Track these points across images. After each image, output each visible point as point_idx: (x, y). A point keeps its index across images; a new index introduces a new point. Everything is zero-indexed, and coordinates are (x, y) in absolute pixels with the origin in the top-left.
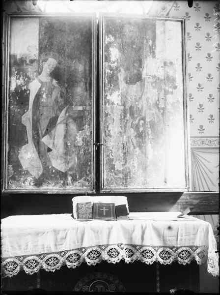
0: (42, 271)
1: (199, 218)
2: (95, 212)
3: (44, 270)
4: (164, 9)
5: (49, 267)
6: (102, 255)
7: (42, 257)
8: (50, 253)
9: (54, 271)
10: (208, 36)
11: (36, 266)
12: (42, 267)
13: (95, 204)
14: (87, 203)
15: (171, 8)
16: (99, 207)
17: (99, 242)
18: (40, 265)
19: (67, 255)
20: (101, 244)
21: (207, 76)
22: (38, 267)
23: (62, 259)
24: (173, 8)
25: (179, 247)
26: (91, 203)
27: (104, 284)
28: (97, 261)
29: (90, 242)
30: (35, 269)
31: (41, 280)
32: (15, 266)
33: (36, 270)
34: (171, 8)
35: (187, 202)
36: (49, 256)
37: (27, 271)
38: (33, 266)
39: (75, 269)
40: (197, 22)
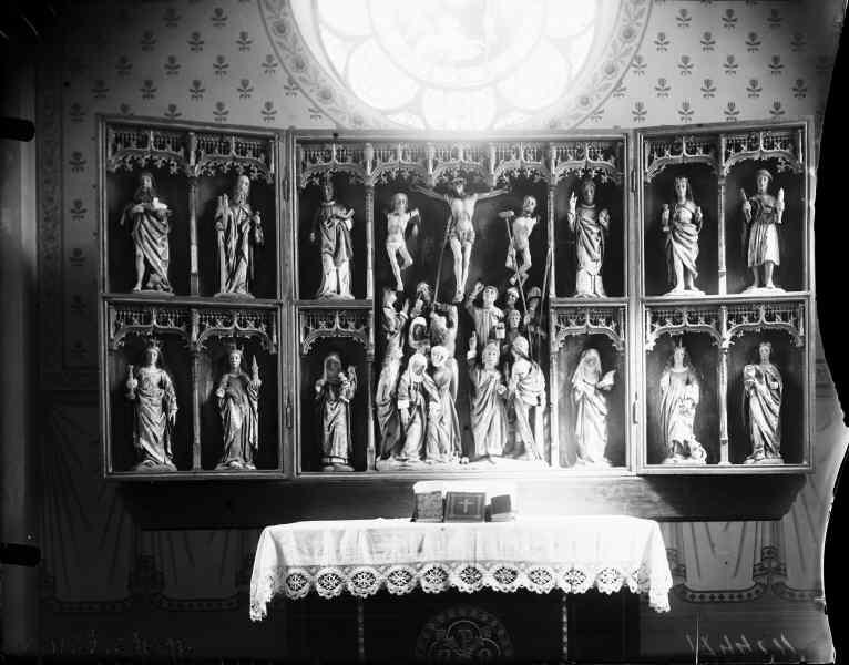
3: (349, 592)
5: (358, 589)
6: (449, 579)
7: (346, 570)
8: (363, 565)
10: (730, 16)
11: (336, 585)
12: (345, 587)
13: (451, 493)
14: (434, 493)
17: (446, 555)
18: (414, 580)
19: (390, 571)
20: (449, 559)
23: (380, 578)
24: (633, 69)
25: (356, 566)
26: (440, 492)
28: (441, 587)
29: (431, 556)
30: (335, 590)
33: (336, 591)
36: (360, 570)
38: (332, 584)
40: (686, 54)
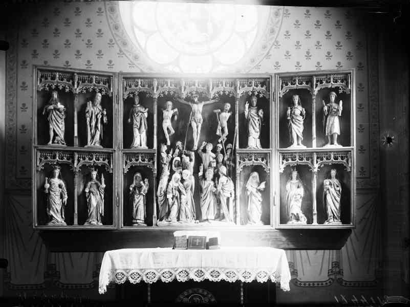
0: (142, 282)
1: (150, 69)
2: (190, 243)
3: (144, 281)
4: (264, 48)
5: (148, 280)
9: (151, 283)
12: (142, 279)
14: (183, 236)
15: (271, 47)
16: (193, 239)
21: (305, 53)
22: (140, 279)
24: (274, 47)
27: (200, 297)
31: (240, 298)
32: (123, 276)
33: (138, 281)
34: (271, 47)
35: (276, 239)
37: (132, 281)
39: (168, 283)
